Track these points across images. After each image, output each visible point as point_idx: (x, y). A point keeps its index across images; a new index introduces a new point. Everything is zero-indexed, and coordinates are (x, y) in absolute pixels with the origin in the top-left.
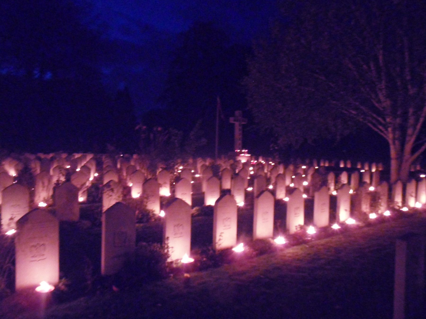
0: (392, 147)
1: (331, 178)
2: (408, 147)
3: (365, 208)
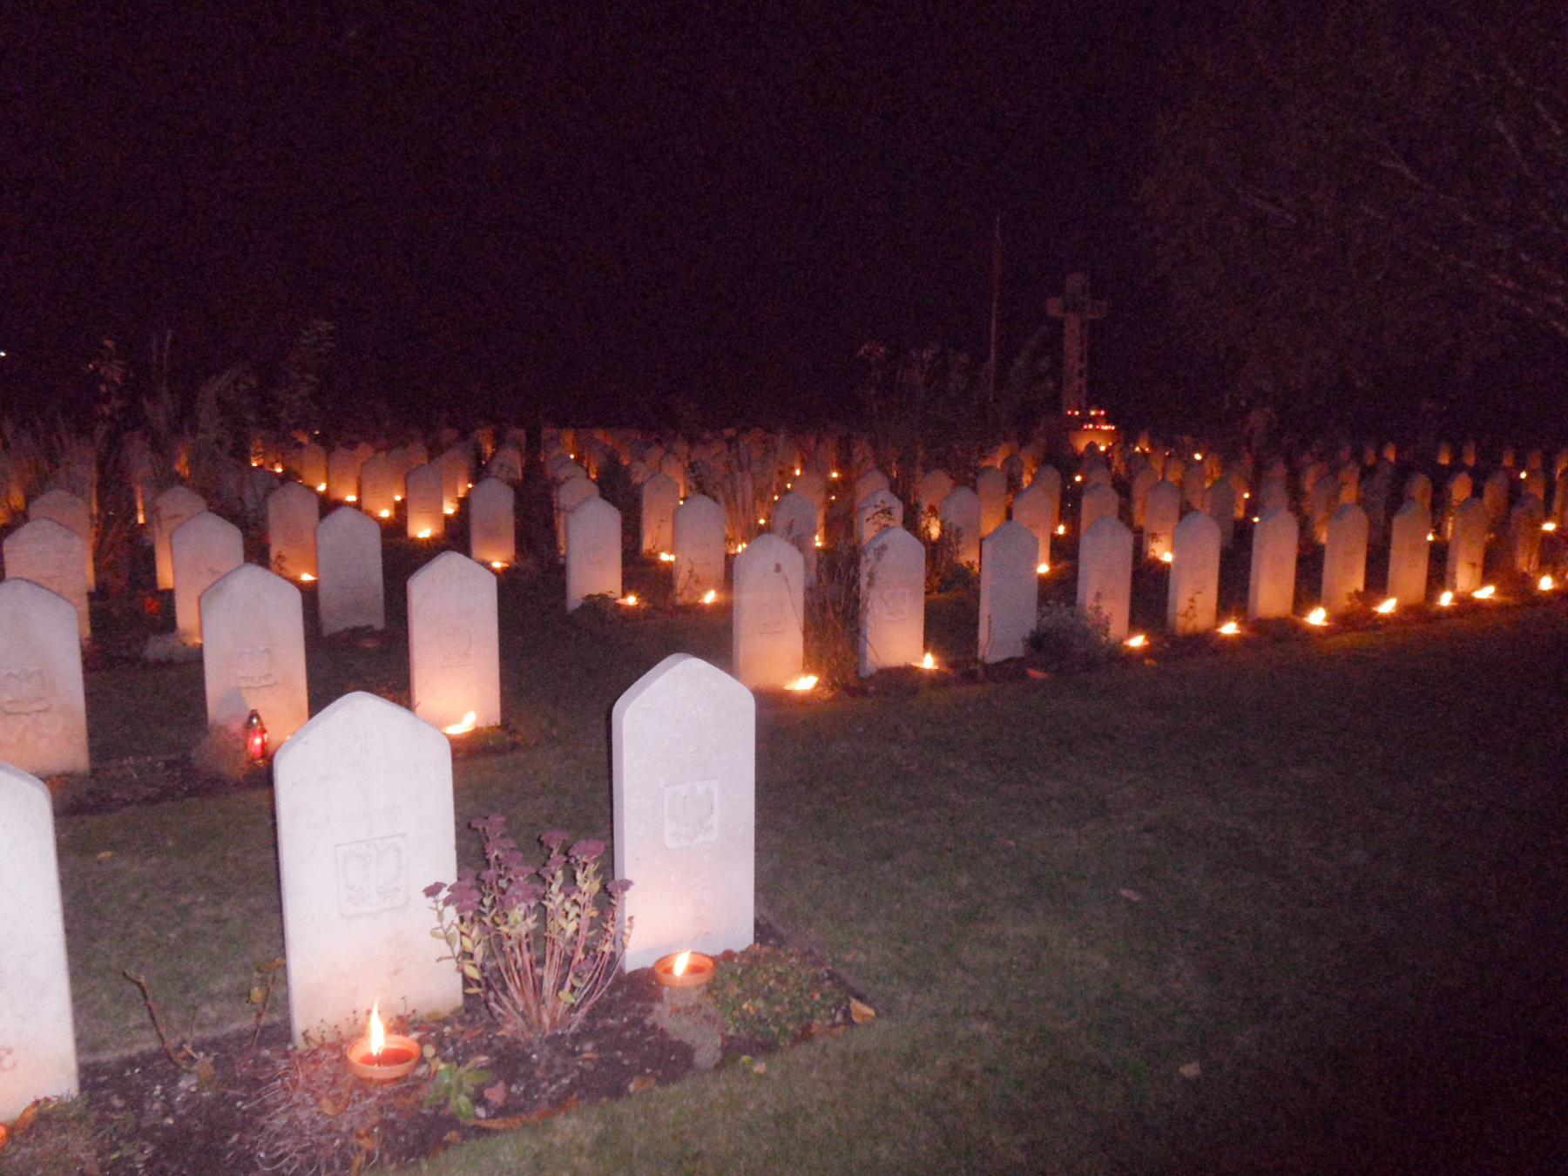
1: (1420, 486)
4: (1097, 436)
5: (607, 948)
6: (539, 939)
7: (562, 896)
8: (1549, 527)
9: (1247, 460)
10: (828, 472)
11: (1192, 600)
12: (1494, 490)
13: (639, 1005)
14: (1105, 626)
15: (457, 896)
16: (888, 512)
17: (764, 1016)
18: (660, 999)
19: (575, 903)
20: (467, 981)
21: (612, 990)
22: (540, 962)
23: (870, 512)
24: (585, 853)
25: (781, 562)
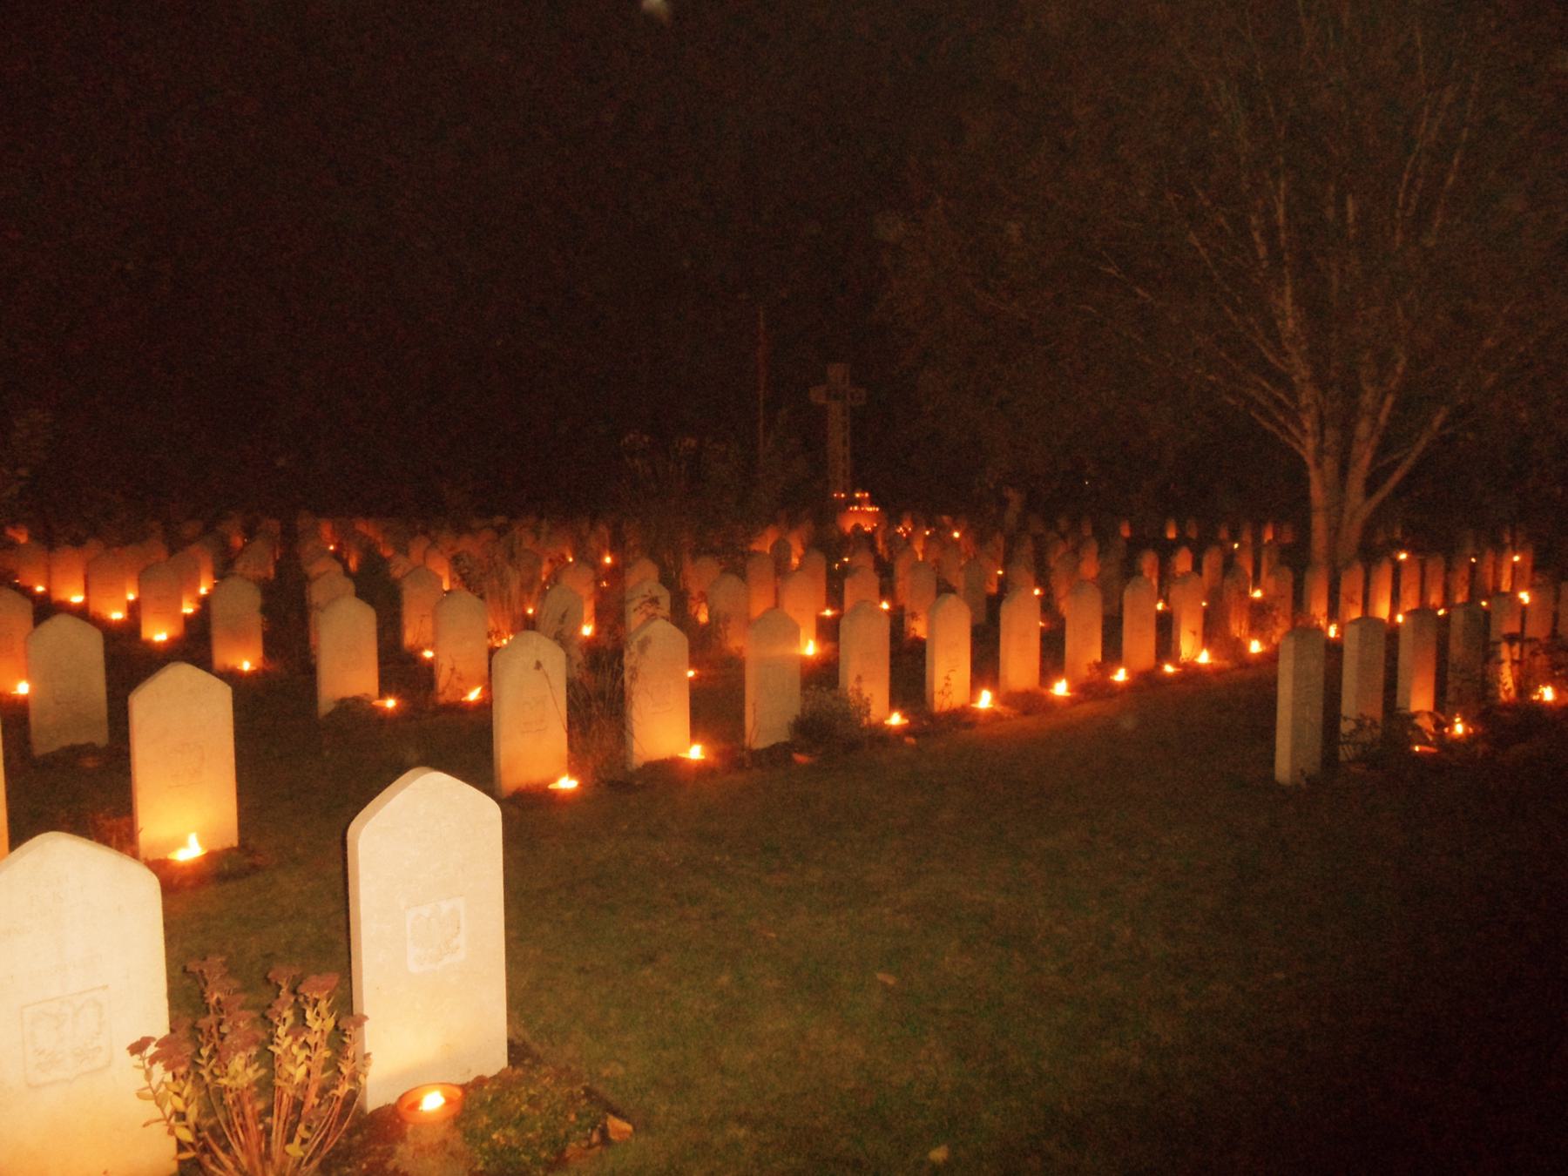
0: (1313, 475)
1: (1148, 561)
2: (1356, 484)
3: (1237, 628)
4: (862, 516)
5: (343, 1089)
6: (266, 1086)
7: (290, 1039)
8: (1258, 594)
9: (999, 539)
10: (600, 556)
11: (948, 678)
12: (1212, 559)
13: (379, 1148)
14: (866, 706)
15: (168, 1052)
16: (654, 601)
17: (514, 1144)
18: (403, 1139)
19: (306, 1044)
20: (181, 1146)
21: (350, 1133)
22: (269, 1111)
23: (635, 604)
24: (318, 991)
25: (541, 659)
